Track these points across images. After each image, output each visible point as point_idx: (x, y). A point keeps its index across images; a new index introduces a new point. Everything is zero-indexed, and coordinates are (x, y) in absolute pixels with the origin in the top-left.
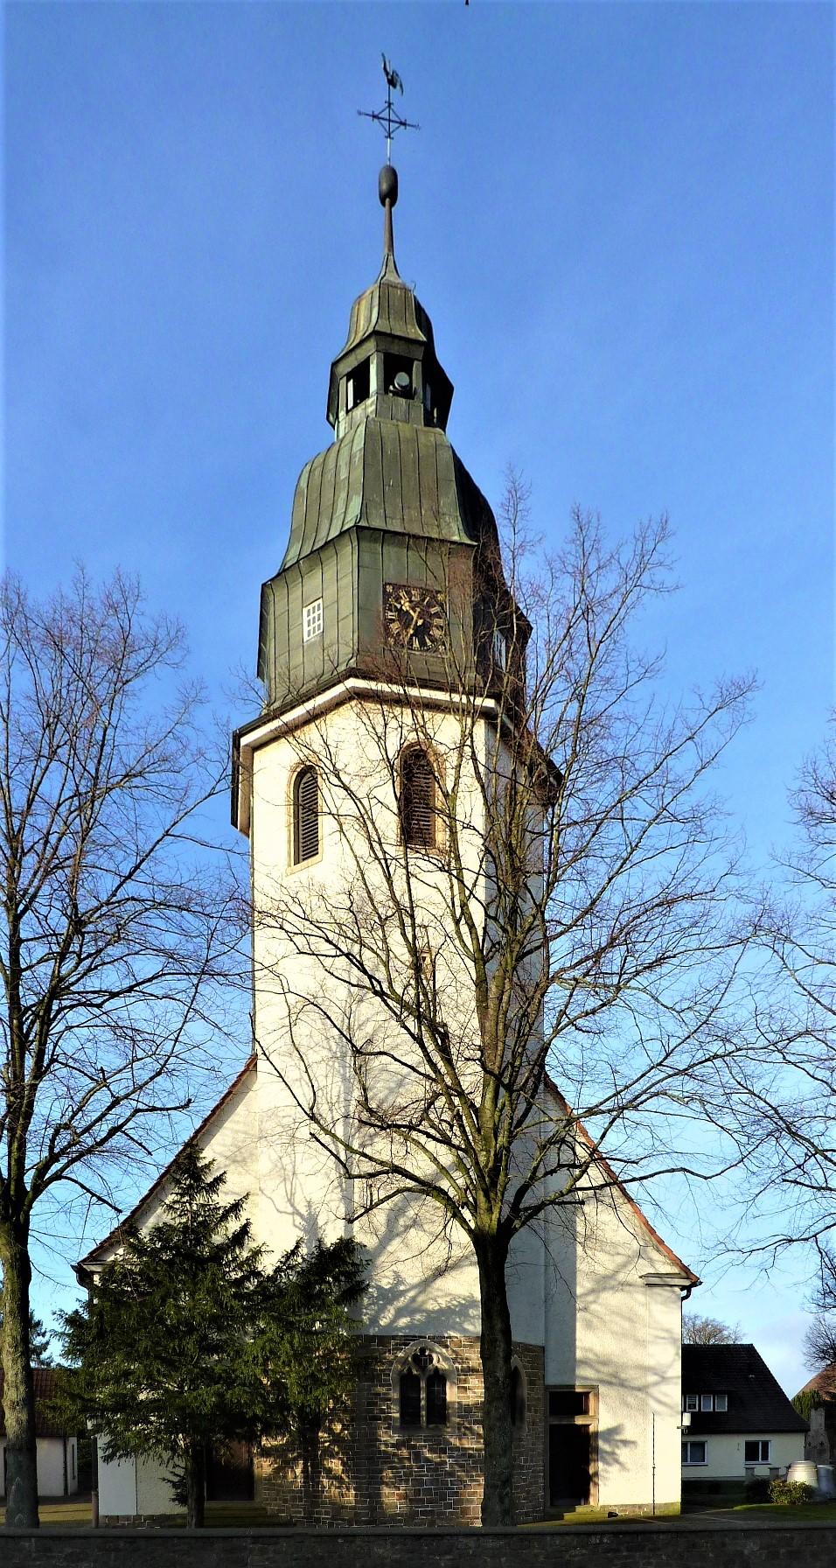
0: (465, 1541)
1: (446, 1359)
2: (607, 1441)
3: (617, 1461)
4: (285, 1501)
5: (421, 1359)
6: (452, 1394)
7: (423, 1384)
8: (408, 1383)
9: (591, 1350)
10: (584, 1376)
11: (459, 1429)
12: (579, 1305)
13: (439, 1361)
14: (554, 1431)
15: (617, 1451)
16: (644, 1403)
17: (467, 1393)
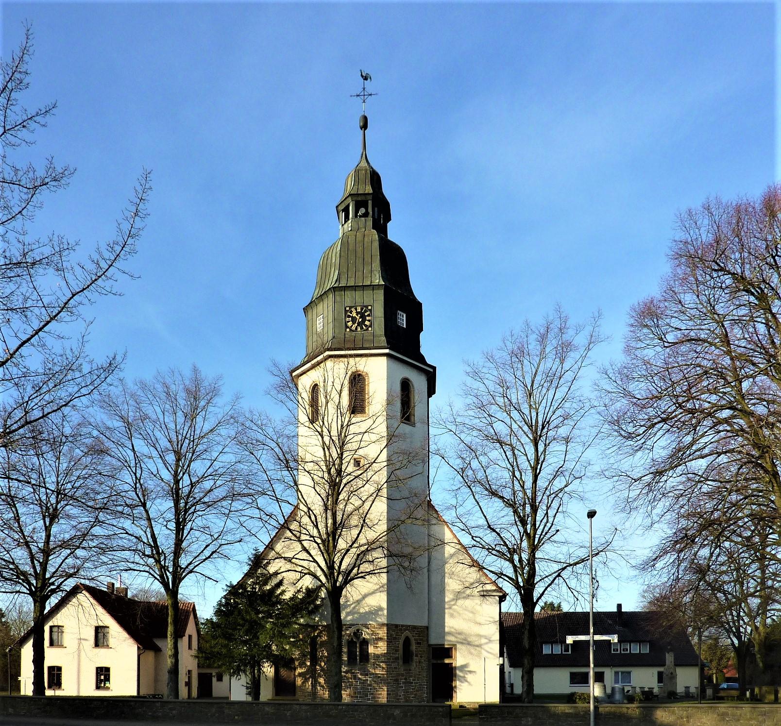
0: (296, 706)
1: (368, 634)
2: (461, 671)
3: (466, 681)
4: (305, 696)
5: (357, 634)
6: (371, 650)
7: (358, 645)
8: (351, 644)
9: (453, 628)
10: (449, 640)
11: (374, 665)
12: (446, 606)
13: (365, 635)
14: (435, 666)
15: (466, 676)
16: (480, 653)
17: (378, 649)
